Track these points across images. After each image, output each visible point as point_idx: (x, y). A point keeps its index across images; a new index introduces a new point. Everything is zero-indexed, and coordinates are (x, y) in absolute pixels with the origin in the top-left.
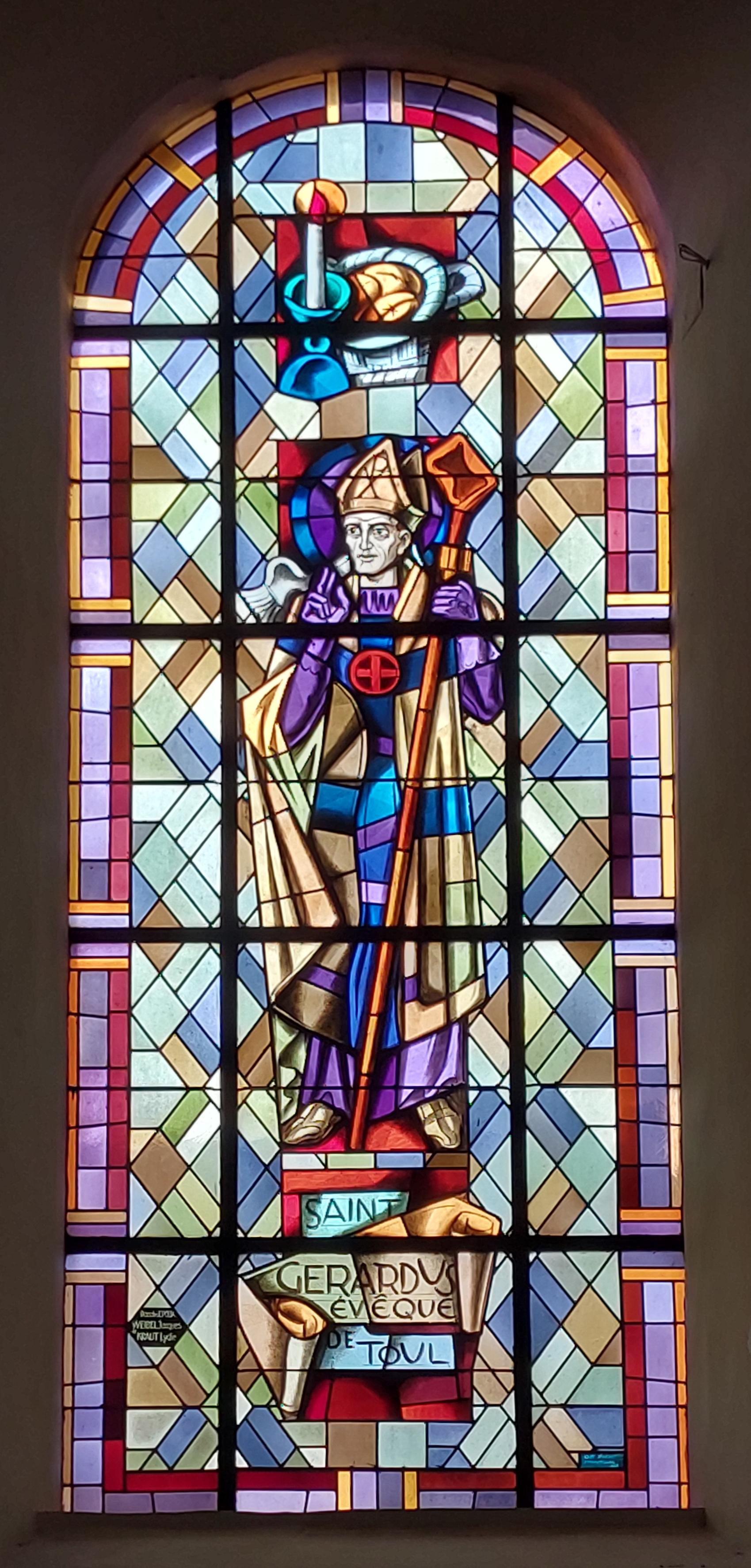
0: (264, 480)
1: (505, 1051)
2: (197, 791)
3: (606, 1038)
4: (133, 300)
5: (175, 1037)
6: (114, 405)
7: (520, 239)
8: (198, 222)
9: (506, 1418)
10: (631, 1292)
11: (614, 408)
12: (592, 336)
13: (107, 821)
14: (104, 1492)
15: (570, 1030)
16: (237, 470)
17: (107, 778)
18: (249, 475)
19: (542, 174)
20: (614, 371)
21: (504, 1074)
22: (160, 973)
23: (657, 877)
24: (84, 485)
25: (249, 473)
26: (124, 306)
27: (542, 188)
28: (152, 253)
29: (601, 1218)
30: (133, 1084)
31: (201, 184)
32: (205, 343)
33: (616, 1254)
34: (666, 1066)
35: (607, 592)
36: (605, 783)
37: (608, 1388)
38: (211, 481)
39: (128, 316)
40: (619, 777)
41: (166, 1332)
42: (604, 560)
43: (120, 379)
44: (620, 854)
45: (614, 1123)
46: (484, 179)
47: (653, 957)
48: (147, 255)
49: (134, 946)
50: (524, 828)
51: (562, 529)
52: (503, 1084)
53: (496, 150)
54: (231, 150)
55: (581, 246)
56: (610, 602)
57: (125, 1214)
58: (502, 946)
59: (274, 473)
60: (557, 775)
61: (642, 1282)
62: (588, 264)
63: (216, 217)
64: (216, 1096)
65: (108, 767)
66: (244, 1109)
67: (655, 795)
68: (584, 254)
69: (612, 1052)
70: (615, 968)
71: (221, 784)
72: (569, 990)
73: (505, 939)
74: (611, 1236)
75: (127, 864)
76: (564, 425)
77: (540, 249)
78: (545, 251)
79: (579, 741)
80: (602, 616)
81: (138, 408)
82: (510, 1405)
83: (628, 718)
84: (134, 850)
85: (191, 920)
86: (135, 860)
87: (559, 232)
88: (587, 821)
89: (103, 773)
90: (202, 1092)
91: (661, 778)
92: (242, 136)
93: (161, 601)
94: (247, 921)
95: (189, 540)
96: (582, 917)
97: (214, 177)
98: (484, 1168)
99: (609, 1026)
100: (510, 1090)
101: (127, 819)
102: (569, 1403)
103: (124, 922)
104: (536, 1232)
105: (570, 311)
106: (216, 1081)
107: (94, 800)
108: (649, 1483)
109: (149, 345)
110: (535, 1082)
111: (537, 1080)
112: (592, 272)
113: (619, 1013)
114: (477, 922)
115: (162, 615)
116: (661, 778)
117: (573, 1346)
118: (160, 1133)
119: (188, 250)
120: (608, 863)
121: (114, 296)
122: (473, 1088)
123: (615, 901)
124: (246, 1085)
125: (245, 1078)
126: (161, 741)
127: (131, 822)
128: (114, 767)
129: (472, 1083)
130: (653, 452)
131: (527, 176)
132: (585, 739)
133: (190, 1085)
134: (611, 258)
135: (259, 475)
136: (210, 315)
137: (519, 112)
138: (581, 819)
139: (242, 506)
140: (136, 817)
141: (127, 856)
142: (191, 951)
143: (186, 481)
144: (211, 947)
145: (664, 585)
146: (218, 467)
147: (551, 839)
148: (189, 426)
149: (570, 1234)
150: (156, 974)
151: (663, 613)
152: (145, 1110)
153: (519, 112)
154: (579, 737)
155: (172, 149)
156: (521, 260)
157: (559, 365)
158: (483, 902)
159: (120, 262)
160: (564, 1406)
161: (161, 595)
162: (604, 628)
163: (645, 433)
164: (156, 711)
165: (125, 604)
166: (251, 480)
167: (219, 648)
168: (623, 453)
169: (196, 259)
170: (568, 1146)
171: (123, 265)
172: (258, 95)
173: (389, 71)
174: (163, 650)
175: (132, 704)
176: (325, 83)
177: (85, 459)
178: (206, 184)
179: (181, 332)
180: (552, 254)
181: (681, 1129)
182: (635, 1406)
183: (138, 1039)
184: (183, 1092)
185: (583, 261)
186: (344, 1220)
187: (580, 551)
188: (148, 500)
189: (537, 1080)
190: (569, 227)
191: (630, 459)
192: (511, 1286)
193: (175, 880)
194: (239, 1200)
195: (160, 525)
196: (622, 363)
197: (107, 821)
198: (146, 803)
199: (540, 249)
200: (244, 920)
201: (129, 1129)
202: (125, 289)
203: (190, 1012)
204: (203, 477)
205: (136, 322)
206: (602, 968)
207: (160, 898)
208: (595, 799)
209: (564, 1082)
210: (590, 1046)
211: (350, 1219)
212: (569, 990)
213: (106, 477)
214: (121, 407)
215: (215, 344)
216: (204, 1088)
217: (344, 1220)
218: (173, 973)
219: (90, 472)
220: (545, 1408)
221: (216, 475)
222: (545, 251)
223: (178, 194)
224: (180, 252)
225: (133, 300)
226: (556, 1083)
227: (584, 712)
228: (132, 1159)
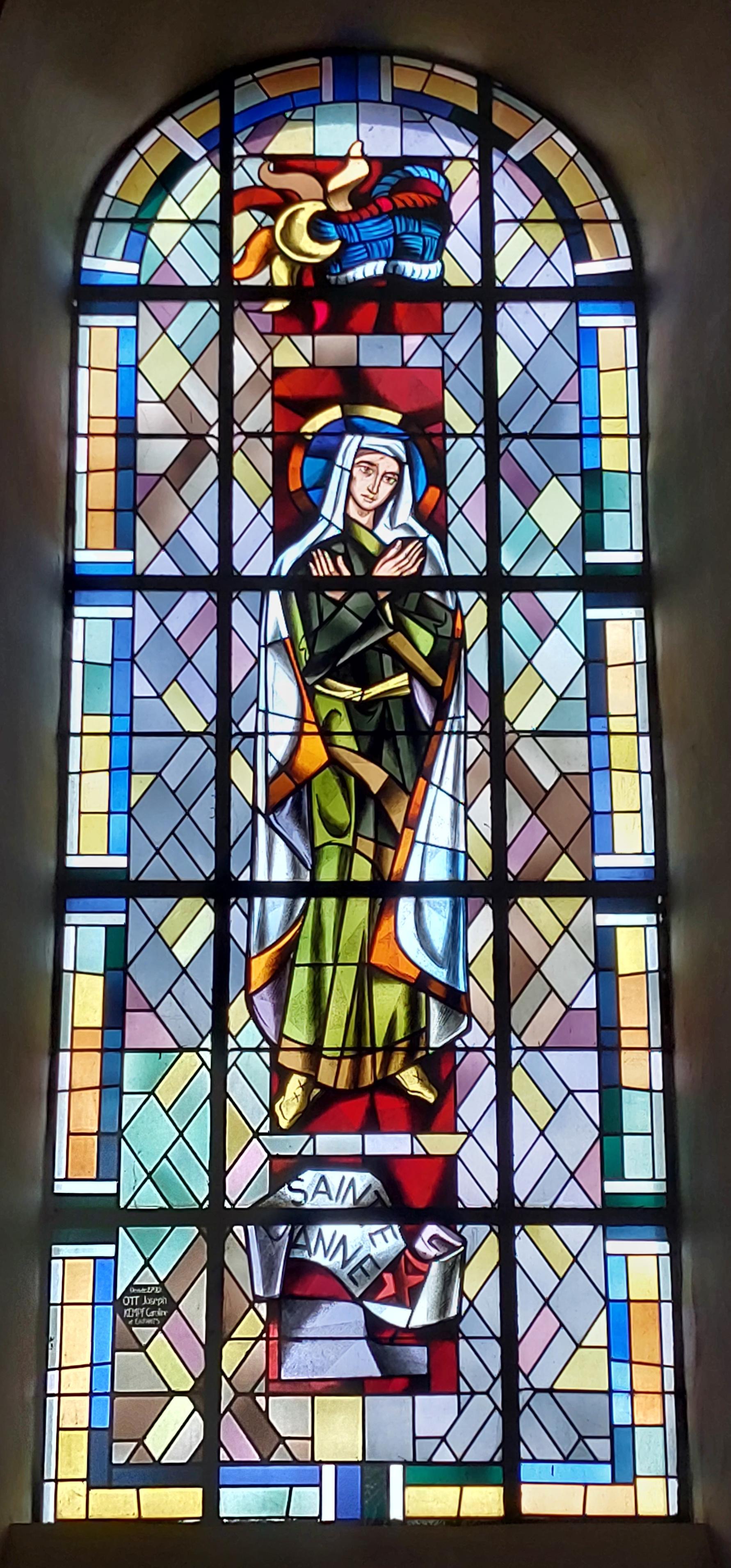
0: (258, 435)
1: (479, 402)
2: (189, 1060)
3: (588, 999)
4: (134, 549)
7: (500, 212)
9: (475, 447)
12: (574, 594)
14: (89, 1488)
16: (233, 726)
19: (517, 153)
21: (478, 422)
22: (165, 259)
24: (85, 737)
25: (246, 427)
26: (126, 556)
28: (160, 217)
32: (207, 305)
33: (574, 305)
39: (136, 278)
41: (155, 1307)
46: (487, 1393)
48: (154, 220)
51: (541, 489)
52: (478, 432)
55: (552, 216)
57: (131, 609)
59: (269, 429)
61: (597, 328)
62: (562, 236)
66: (234, 1073)
69: (594, 1012)
73: (490, 896)
75: (126, 816)
77: (516, 220)
78: (522, 222)
81: (128, 1134)
82: (497, 1392)
85: (195, 279)
87: (534, 206)
88: (569, 777)
89: (110, 426)
90: (194, 1054)
92: (242, 112)
94: (242, 570)
95: (184, 952)
98: (460, 510)
99: (591, 987)
104: (502, 283)
105: (548, 279)
108: (635, 1476)
110: (528, 1386)
111: (521, 1042)
114: (461, 877)
117: (535, 386)
118: (152, 1097)
119: (193, 217)
122: (461, 1049)
123: (606, 1183)
126: (164, 398)
127: (136, 474)
128: (106, 1031)
130: (655, 1258)
135: (254, 430)
136: (213, 278)
137: (497, 93)
139: (238, 459)
140: (140, 470)
141: (133, 363)
142: (189, 904)
153: (497, 93)
154: (553, 398)
156: (501, 232)
158: (469, 861)
161: (164, 331)
166: (249, 435)
167: (212, 904)
170: (540, 643)
177: (82, 810)
181: (667, 1198)
186: (330, 1198)
189: (521, 1042)
192: (494, 1093)
194: (494, 1104)
199: (516, 220)
200: (239, 570)
209: (547, 1045)
211: (337, 1198)
213: (112, 429)
217: (330, 1198)
218: (178, 331)
219: (99, 427)
222: (522, 222)
225: (134, 549)
228: (129, 960)
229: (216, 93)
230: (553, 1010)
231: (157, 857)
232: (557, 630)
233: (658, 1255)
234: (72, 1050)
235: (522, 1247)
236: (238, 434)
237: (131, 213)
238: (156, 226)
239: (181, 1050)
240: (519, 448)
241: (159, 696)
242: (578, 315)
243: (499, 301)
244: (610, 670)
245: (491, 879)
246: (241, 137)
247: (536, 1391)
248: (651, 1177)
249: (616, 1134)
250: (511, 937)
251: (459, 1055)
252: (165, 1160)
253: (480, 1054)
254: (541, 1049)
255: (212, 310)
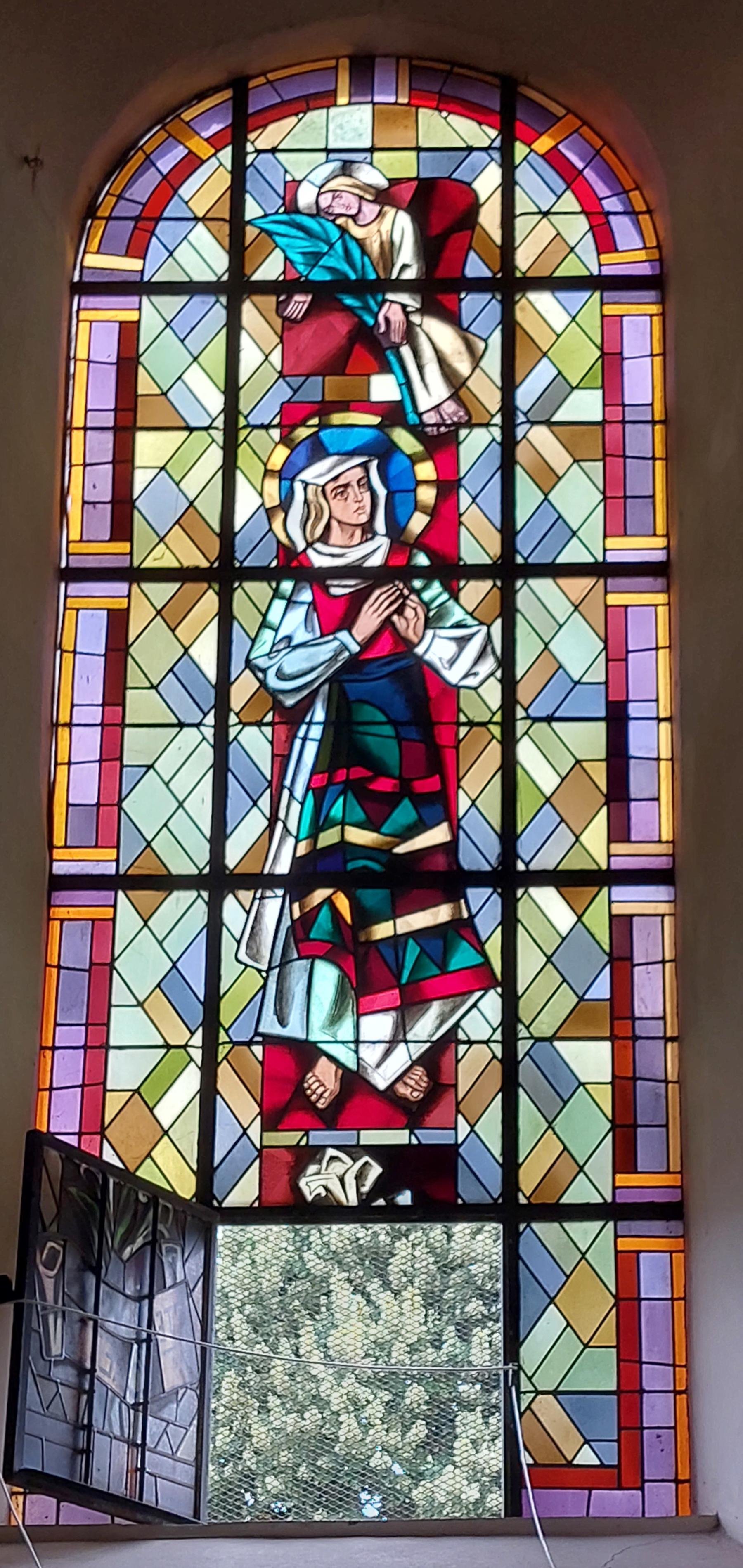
0: (266, 427)
2: (190, 735)
3: (602, 989)
5: (158, 990)
6: (122, 355)
7: (522, 203)
8: (207, 187)
10: (627, 1265)
11: (611, 362)
13: (79, 1089)
15: (564, 980)
17: (82, 1043)
18: (252, 422)
20: (611, 326)
23: (657, 821)
26: (135, 264)
27: (543, 156)
28: (165, 215)
29: (594, 1184)
30: (112, 1043)
31: (214, 155)
33: (602, 581)
34: (653, 497)
35: (605, 536)
36: (603, 725)
37: (601, 1373)
38: (216, 428)
40: (617, 718)
42: (602, 504)
43: (129, 333)
44: (618, 794)
45: (609, 1079)
47: (645, 901)
48: (159, 219)
49: (121, 894)
50: (519, 771)
52: (493, 422)
53: (499, 126)
54: (246, 126)
56: (612, 852)
58: (495, 891)
60: (557, 715)
62: (587, 227)
63: (229, 183)
64: (197, 1055)
65: (100, 708)
67: (651, 740)
68: (582, 218)
70: (611, 917)
71: (214, 727)
72: (564, 939)
74: (592, 276)
76: (569, 1152)
77: (540, 212)
78: (546, 214)
79: (577, 683)
80: (600, 559)
83: (626, 660)
84: (123, 795)
85: (180, 866)
86: (125, 805)
89: (96, 714)
91: (659, 720)
93: (146, 929)
96: (575, 863)
97: (229, 149)
100: (502, 428)
101: (118, 763)
102: (560, 1389)
103: (110, 869)
104: (526, 559)
106: (198, 1039)
107: (86, 744)
109: (160, 300)
112: (590, 235)
113: (618, 1130)
115: (160, 558)
116: (659, 720)
120: (608, 968)
121: (127, 254)
124: (227, 1040)
125: (226, 1031)
127: (122, 766)
128: (107, 708)
129: (463, 719)
131: (529, 145)
132: (584, 680)
133: (172, 1043)
134: (608, 222)
138: (578, 762)
139: (224, 1070)
141: (109, 961)
142: (181, 898)
143: (191, 429)
144: (199, 896)
145: (661, 529)
146: (222, 416)
147: (548, 782)
148: (195, 377)
149: (562, 1201)
150: (142, 923)
151: (659, 556)
152: (123, 1072)
155: (187, 123)
157: (558, 318)
159: (131, 224)
160: (555, 1393)
162: (602, 570)
163: (642, 383)
164: (151, 650)
165: (124, 547)
166: (259, 152)
167: (207, 899)
168: (629, 1015)
169: (209, 223)
171: (135, 228)
172: (270, 76)
173: (398, 58)
174: (161, 592)
175: (128, 647)
176: (336, 67)
178: (219, 155)
179: (189, 288)
180: (553, 218)
182: (629, 1392)
183: (119, 993)
184: (164, 1051)
185: (582, 224)
187: (579, 495)
188: (150, 448)
190: (569, 193)
191: (645, 1431)
193: (165, 825)
195: (163, 472)
196: (635, 1255)
197: (83, 1028)
198: (136, 745)
199: (540, 212)
201: (105, 1090)
202: (137, 248)
203: (191, 504)
204: (206, 424)
205: (146, 279)
206: (598, 918)
207: (149, 844)
208: (589, 740)
210: (586, 997)
212: (563, 779)
213: (111, 424)
214: (128, 363)
215: (205, 894)
216: (197, 725)
218: (161, 921)
220: (533, 1395)
221: (220, 423)
223: (191, 164)
224: (191, 215)
226: (548, 717)
227: (579, 651)
229: (228, 94)
230: (566, 1000)
231: (146, 929)
232: (575, 539)
233: (671, 1252)
234: (85, 429)
235: (523, 599)
236: (245, 427)
237: (136, 210)
238: (161, 224)
239: (181, 725)
240: (540, 436)
241: (165, 394)
242: (606, 592)
243: (521, 886)
244: (636, 969)
245: (500, 1201)
246: (252, 136)
247: (538, 1392)
248: (665, 1170)
249: (636, 1362)
250: (521, 1263)
251: (463, 731)
252: (171, 674)
253: (485, 1046)
254: (549, 719)
255: (200, 900)
